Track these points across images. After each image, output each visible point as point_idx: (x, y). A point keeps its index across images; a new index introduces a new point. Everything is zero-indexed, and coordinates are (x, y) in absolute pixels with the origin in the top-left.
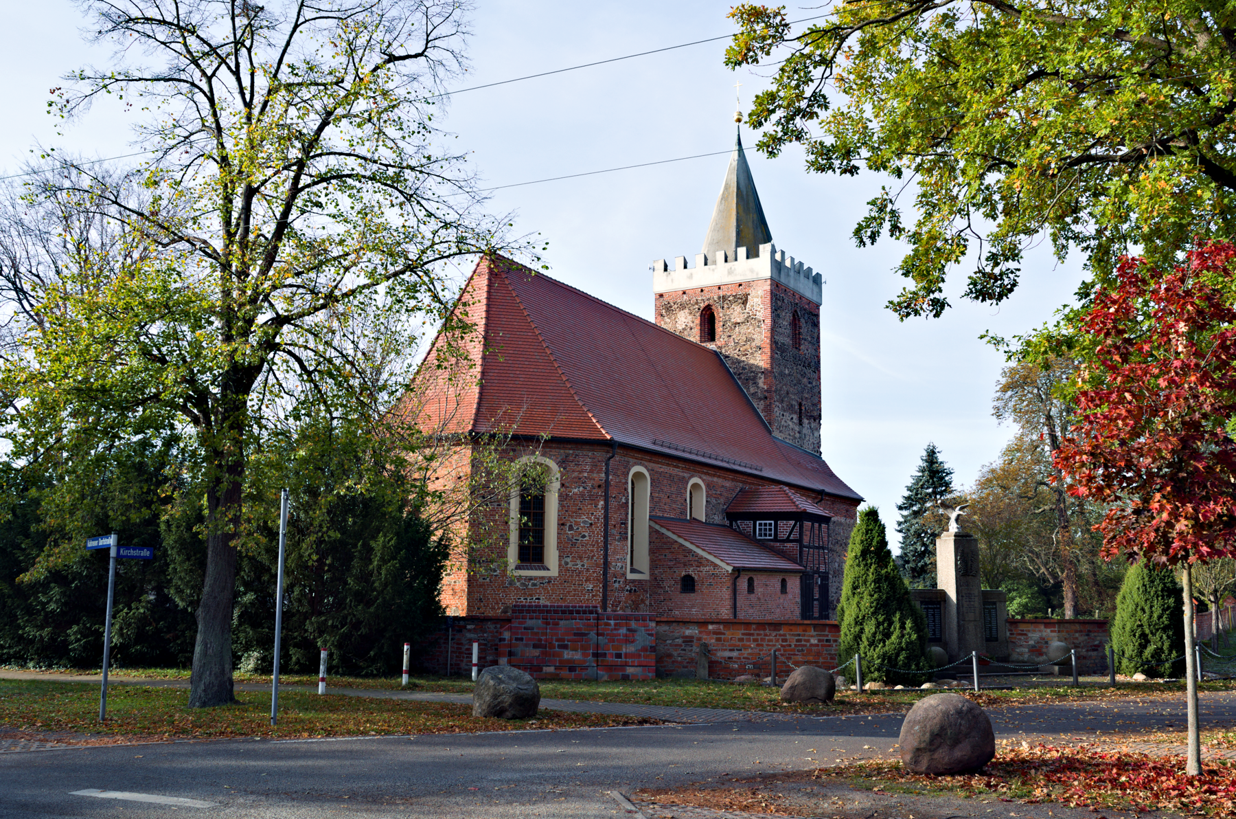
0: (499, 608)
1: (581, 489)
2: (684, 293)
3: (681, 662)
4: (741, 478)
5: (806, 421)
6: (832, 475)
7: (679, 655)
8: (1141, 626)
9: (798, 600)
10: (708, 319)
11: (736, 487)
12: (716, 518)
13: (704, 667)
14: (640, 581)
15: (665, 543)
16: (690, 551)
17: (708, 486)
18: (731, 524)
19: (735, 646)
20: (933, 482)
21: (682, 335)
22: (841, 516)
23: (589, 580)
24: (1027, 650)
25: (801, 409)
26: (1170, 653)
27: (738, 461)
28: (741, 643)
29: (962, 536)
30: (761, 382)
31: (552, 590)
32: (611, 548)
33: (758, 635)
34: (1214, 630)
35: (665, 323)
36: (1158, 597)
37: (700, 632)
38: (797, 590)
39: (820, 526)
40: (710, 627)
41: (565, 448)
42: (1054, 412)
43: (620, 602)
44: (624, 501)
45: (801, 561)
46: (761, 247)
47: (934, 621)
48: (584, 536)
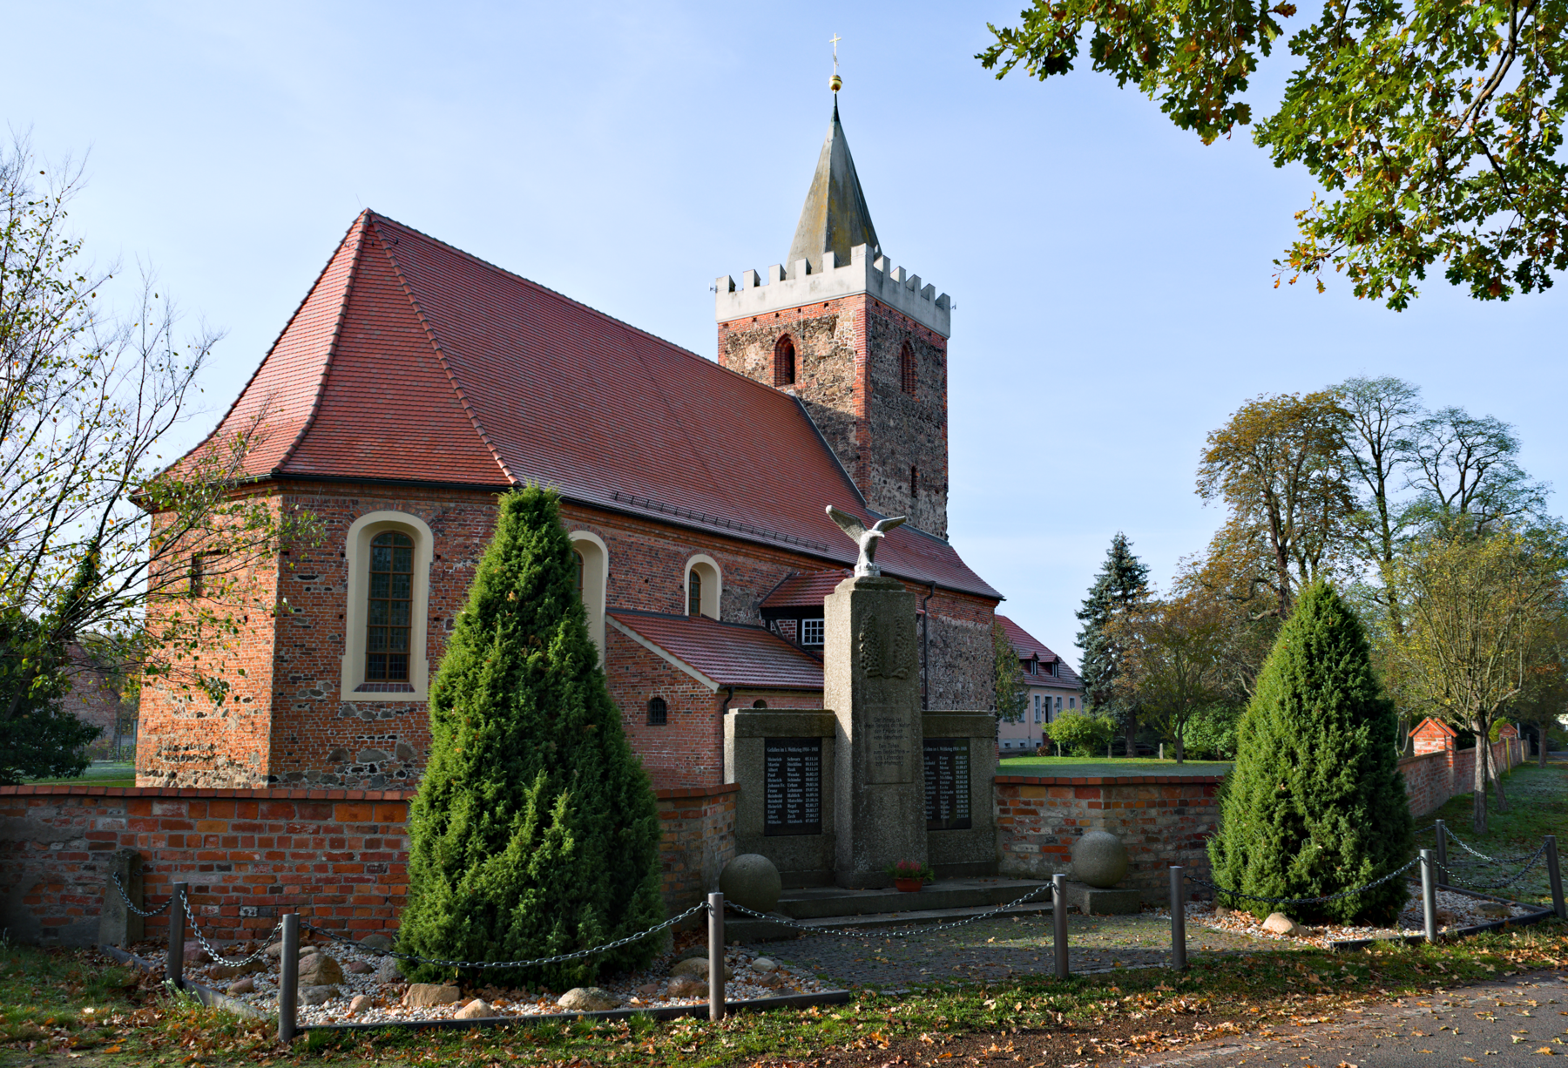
2: (755, 320)
3: (83, 900)
4: (786, 558)
5: (922, 493)
6: (960, 565)
7: (79, 882)
8: (1287, 795)
10: (785, 354)
12: (742, 615)
13: (116, 915)
15: (627, 649)
16: (661, 660)
17: (727, 568)
18: (768, 625)
19: (215, 857)
20: (1122, 583)
21: (752, 377)
22: (968, 619)
24: (1036, 848)
25: (914, 477)
26: (1355, 868)
27: (804, 539)
28: (229, 851)
29: (877, 587)
30: (853, 438)
31: (417, 723)
33: (273, 828)
34: (1479, 786)
35: (731, 362)
36: (1328, 723)
37: (132, 823)
40: (157, 809)
41: (440, 500)
42: (1278, 489)
46: (854, 250)
47: (802, 785)
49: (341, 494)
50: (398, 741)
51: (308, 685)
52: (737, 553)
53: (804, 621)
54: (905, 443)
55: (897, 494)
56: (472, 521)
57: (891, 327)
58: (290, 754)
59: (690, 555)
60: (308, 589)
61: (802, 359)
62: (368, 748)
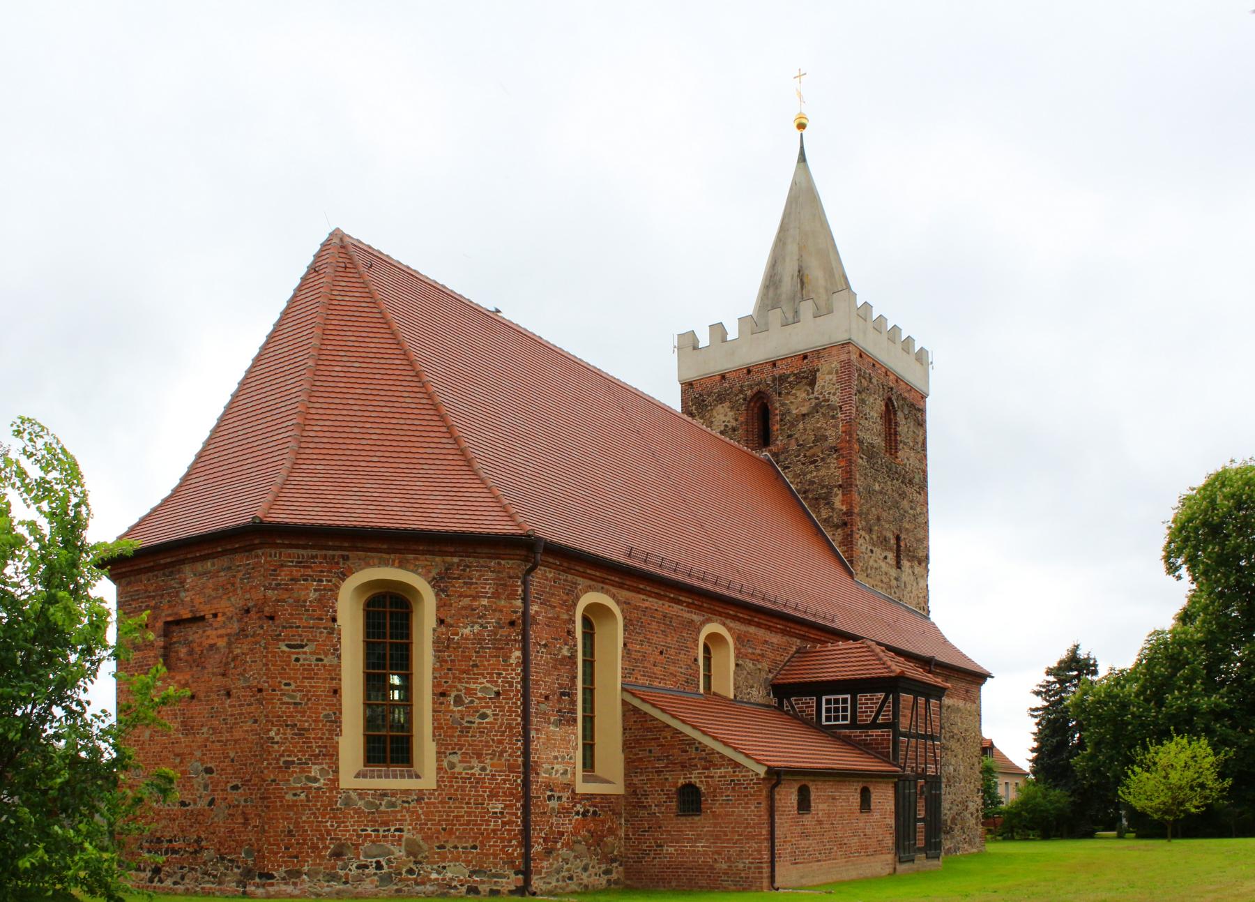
0: (326, 848)
1: (477, 628)
5: (906, 563)
9: (891, 821)
11: (790, 645)
12: (754, 692)
14: (604, 797)
15: (649, 730)
16: (692, 742)
17: (739, 639)
18: (781, 703)
23: (496, 795)
25: (898, 546)
32: (538, 740)
38: (890, 806)
39: (927, 701)
43: (562, 834)
44: (565, 652)
45: (896, 757)
48: (484, 716)
49: (329, 548)
50: (406, 835)
51: (303, 771)
52: (750, 623)
53: (824, 699)
54: (890, 509)
55: (883, 564)
56: (479, 579)
57: (874, 381)
58: (287, 848)
59: (703, 623)
60: (297, 660)
61: (778, 418)
62: (373, 842)
